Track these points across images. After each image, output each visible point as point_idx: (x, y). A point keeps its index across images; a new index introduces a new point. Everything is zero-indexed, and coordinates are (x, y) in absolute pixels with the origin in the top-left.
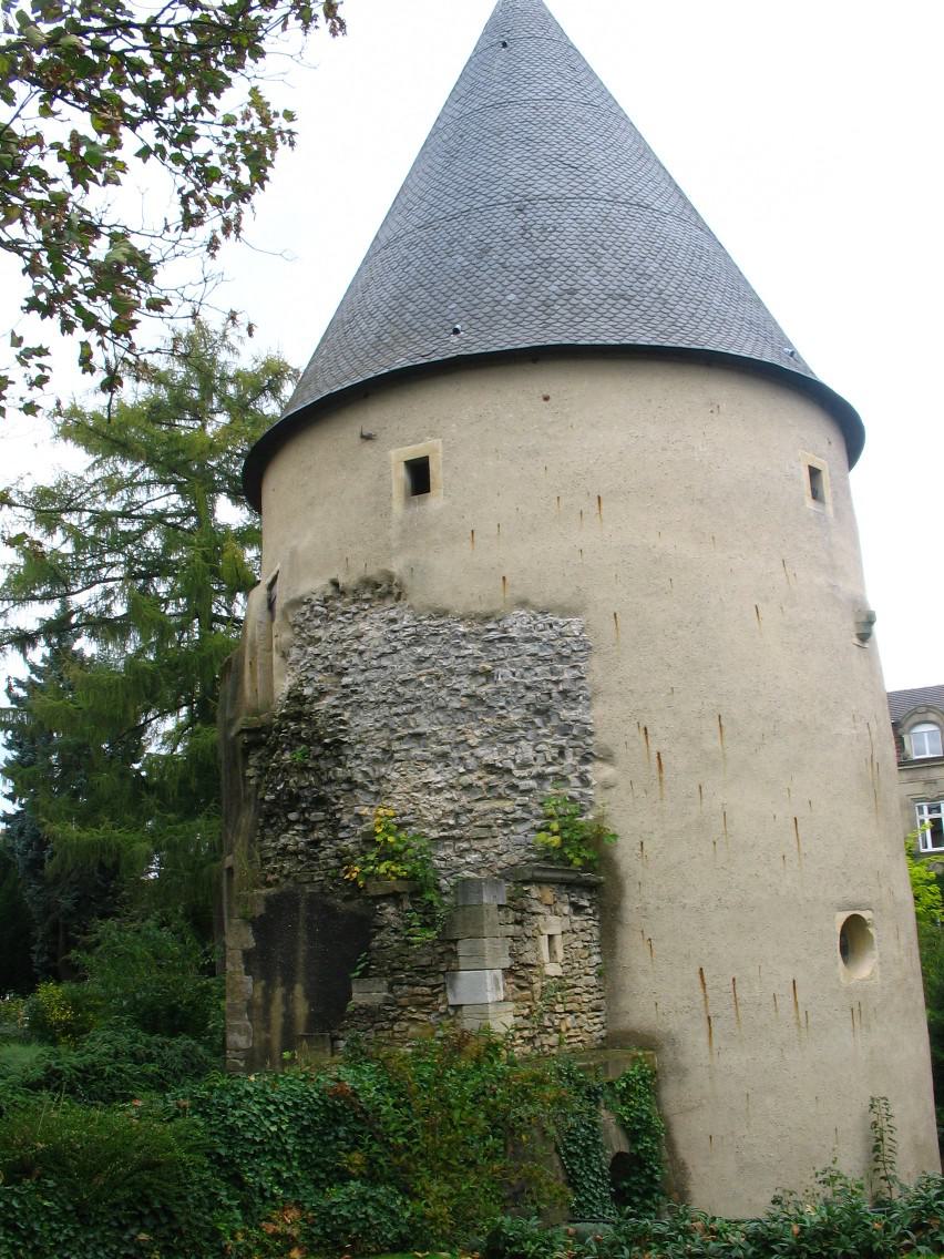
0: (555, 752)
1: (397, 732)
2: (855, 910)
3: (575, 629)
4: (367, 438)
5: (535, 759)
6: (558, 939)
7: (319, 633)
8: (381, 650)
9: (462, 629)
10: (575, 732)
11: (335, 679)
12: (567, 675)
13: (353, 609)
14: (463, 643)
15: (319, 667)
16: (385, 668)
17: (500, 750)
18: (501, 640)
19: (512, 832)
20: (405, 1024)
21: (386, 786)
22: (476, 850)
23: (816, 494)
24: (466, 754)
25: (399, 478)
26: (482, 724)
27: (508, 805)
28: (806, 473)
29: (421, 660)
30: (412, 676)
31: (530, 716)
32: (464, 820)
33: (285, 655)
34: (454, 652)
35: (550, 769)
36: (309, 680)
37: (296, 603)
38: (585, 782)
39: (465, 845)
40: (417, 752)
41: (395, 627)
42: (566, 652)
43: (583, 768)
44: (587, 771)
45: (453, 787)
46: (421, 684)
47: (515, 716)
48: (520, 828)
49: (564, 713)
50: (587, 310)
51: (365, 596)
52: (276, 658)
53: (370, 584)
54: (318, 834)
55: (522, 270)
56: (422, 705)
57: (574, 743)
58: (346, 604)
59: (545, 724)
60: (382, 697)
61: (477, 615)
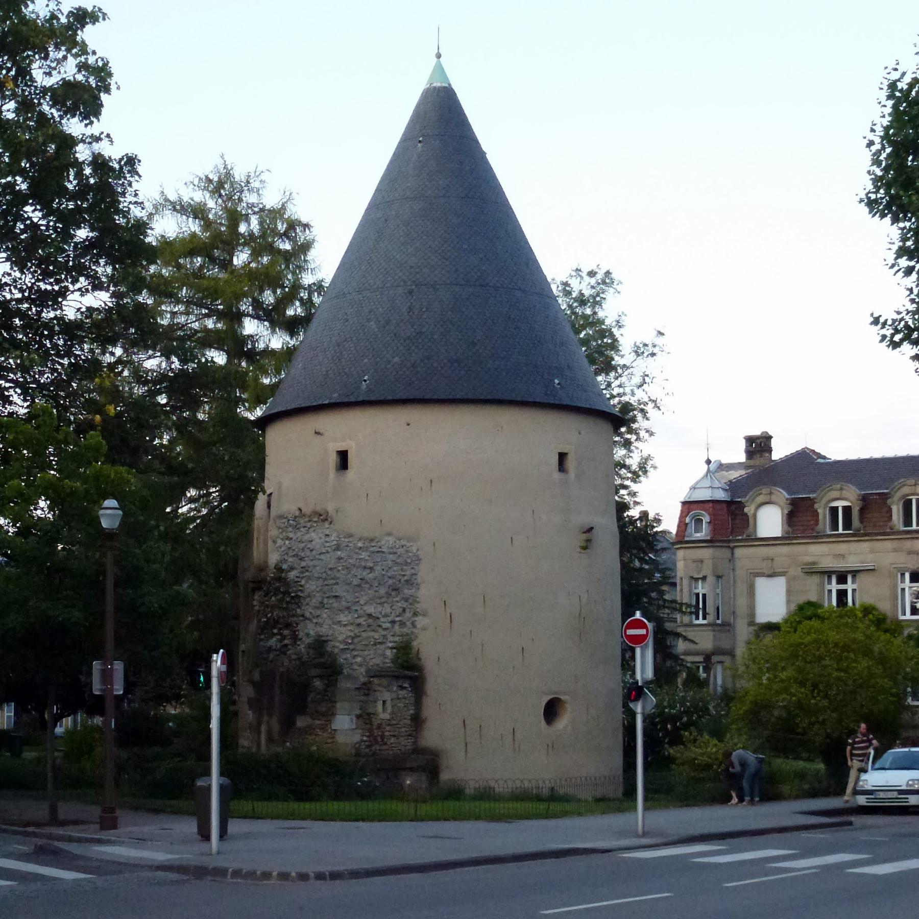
2: (556, 694)
3: (414, 549)
7: (291, 535)
9: (360, 545)
11: (299, 561)
12: (408, 573)
13: (309, 524)
22: (361, 656)
24: (358, 608)
25: (333, 459)
29: (340, 558)
32: (356, 640)
33: (274, 542)
35: (398, 619)
36: (286, 561)
37: (281, 517)
38: (414, 625)
39: (356, 653)
41: (327, 539)
45: (352, 624)
46: (339, 571)
47: (382, 591)
48: (382, 647)
49: (406, 591)
52: (270, 543)
58: (306, 522)
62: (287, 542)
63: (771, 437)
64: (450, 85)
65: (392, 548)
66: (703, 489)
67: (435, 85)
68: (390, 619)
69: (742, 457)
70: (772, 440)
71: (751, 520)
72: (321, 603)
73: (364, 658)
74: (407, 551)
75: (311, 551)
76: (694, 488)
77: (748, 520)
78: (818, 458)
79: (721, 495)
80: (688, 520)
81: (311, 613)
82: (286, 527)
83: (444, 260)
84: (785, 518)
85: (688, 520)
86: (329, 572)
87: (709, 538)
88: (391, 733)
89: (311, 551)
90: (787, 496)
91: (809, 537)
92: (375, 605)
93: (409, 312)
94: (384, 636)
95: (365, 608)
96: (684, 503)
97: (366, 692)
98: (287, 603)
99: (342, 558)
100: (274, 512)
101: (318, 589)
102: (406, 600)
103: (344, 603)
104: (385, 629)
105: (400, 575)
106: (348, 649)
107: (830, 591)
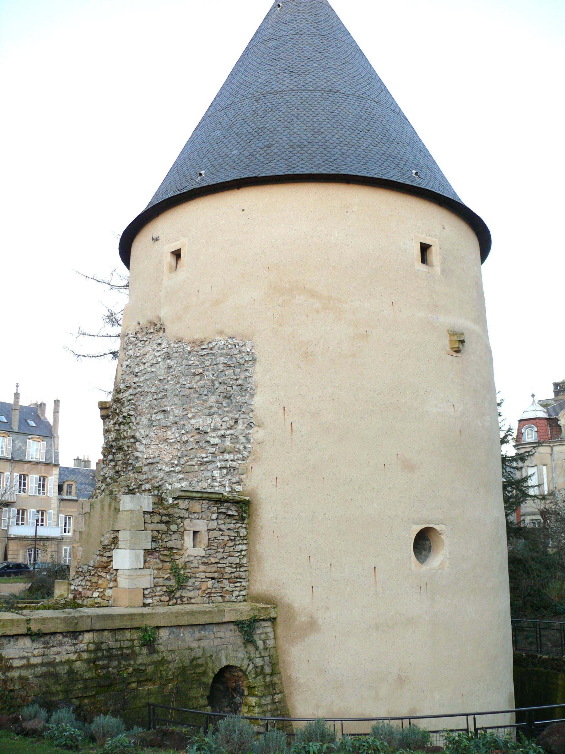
0: (232, 422)
1: (155, 409)
2: (428, 524)
5: (221, 426)
23: (424, 260)
29: (169, 367)
30: (165, 377)
31: (221, 400)
38: (247, 437)
39: (181, 476)
42: (242, 361)
44: (249, 434)
46: (168, 381)
51: (150, 331)
57: (242, 416)
69: (552, 396)
74: (240, 352)
79: (541, 414)
87: (537, 441)
95: (193, 421)
106: (174, 471)
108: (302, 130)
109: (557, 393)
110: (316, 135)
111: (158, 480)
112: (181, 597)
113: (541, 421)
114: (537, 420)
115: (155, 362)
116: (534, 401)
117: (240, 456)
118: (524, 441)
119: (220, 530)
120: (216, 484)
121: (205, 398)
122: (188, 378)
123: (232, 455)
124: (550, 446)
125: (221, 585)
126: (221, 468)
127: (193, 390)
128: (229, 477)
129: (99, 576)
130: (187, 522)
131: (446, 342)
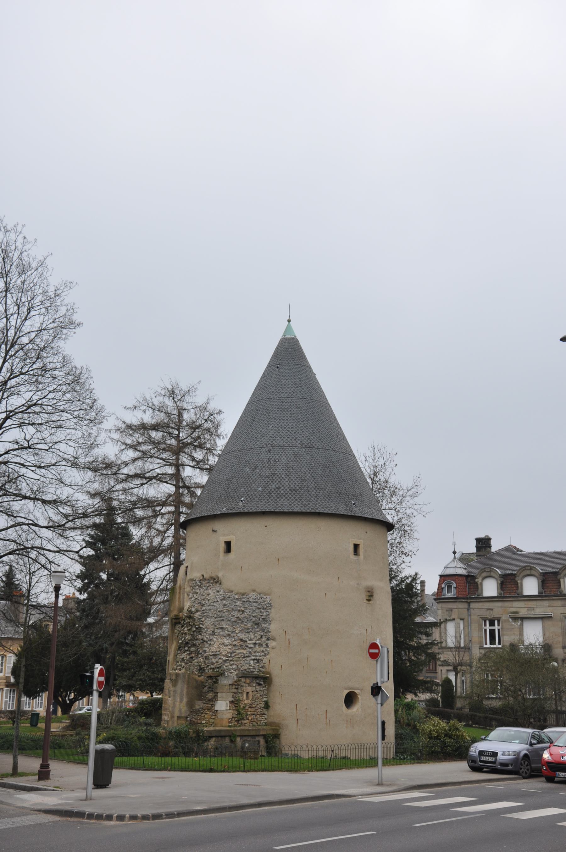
0: (259, 637)
3: (268, 600)
4: (214, 531)
6: (250, 693)
7: (197, 591)
8: (214, 600)
9: (236, 597)
10: (266, 631)
11: (201, 607)
12: (264, 614)
13: (208, 585)
14: (236, 601)
15: (197, 602)
16: (215, 606)
17: (244, 635)
18: (247, 601)
19: (246, 660)
20: (204, 714)
21: (212, 643)
22: (235, 664)
24: (235, 635)
25: (223, 546)
26: (240, 627)
27: (245, 652)
28: (353, 546)
29: (225, 605)
30: (222, 609)
31: (254, 625)
32: (233, 655)
33: (188, 595)
34: (234, 604)
35: (257, 642)
36: (194, 606)
37: (192, 580)
38: (267, 645)
39: (232, 662)
40: (221, 633)
41: (218, 594)
42: (265, 607)
43: (267, 642)
45: (231, 645)
46: (224, 612)
47: (249, 625)
48: (248, 659)
49: (263, 625)
50: (282, 496)
52: (186, 595)
53: (212, 578)
54: (193, 655)
55: (265, 478)
56: (224, 619)
57: (265, 634)
58: (206, 583)
59: (258, 628)
60: (213, 615)
61: (241, 593)
62: (195, 595)
63: (490, 539)
64: (295, 336)
65: (255, 599)
66: (452, 569)
67: (287, 336)
68: (254, 642)
69: (474, 550)
70: (491, 540)
71: (479, 586)
72: (213, 632)
73: (237, 666)
74: (264, 601)
75: (209, 600)
76: (446, 567)
77: (478, 586)
78: (518, 551)
80: (443, 586)
81: (207, 638)
82: (195, 586)
83: (289, 433)
84: (499, 586)
85: (443, 586)
86: (218, 613)
87: (455, 596)
88: (252, 713)
89: (209, 600)
90: (500, 573)
91: (513, 597)
92: (245, 633)
93: (268, 462)
94: (250, 652)
95: (239, 635)
96: (441, 576)
97: (236, 687)
98: (194, 632)
99: (226, 605)
100: (189, 577)
101: (212, 623)
102: (263, 630)
103: (227, 632)
104: (250, 648)
105: (259, 615)
107: (485, 630)
108: (295, 478)
109: (478, 547)
110: (303, 482)
111: (218, 663)
112: (242, 723)
113: (460, 578)
114: (456, 577)
115: (216, 600)
116: (455, 557)
117: (263, 654)
118: (443, 595)
119: (257, 691)
120: (251, 668)
121: (246, 623)
122: (236, 612)
123: (259, 654)
124: (467, 602)
125: (257, 717)
126: (254, 660)
127: (238, 619)
128: (258, 664)
129: (206, 713)
130: (244, 688)
131: (364, 596)
